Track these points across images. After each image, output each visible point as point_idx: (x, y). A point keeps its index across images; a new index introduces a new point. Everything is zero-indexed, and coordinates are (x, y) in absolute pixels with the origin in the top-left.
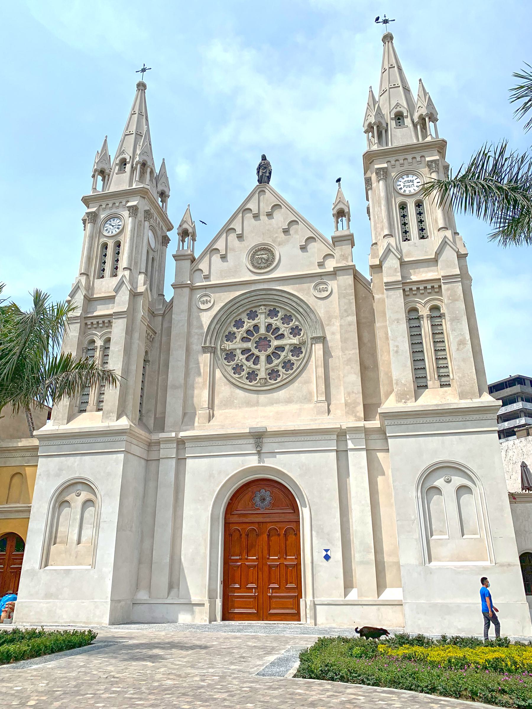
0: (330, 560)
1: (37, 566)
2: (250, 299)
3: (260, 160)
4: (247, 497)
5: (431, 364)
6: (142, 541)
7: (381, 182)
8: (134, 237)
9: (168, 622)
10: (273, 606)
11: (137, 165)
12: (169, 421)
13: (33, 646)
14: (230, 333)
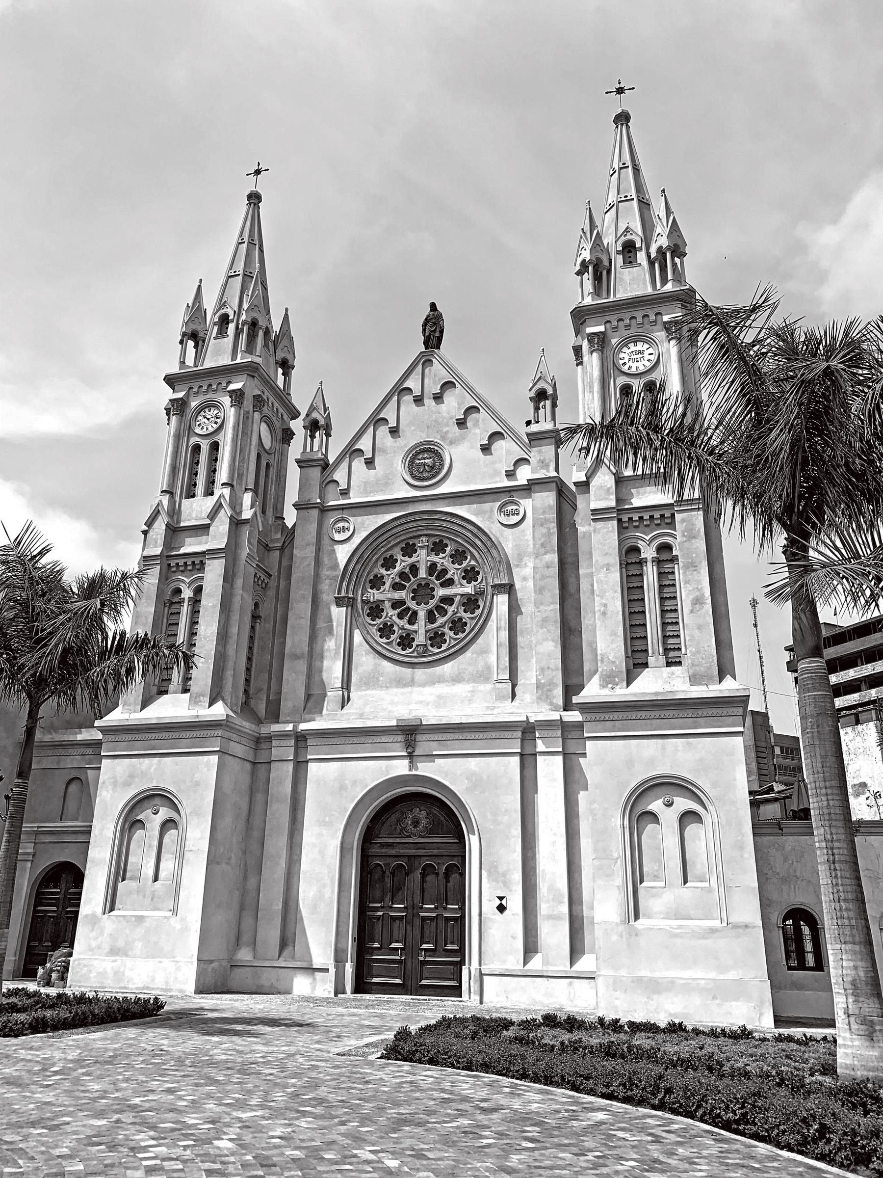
0: (506, 913)
1: (99, 910)
2: (406, 526)
3: (427, 311)
4: (393, 818)
5: (655, 631)
6: (245, 878)
7: (595, 354)
8: (237, 436)
9: (280, 993)
10: (425, 974)
11: (243, 326)
12: (286, 706)
13: (77, 1014)
14: (376, 576)
